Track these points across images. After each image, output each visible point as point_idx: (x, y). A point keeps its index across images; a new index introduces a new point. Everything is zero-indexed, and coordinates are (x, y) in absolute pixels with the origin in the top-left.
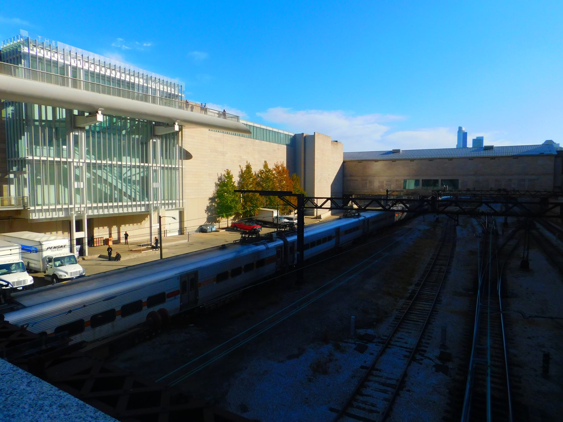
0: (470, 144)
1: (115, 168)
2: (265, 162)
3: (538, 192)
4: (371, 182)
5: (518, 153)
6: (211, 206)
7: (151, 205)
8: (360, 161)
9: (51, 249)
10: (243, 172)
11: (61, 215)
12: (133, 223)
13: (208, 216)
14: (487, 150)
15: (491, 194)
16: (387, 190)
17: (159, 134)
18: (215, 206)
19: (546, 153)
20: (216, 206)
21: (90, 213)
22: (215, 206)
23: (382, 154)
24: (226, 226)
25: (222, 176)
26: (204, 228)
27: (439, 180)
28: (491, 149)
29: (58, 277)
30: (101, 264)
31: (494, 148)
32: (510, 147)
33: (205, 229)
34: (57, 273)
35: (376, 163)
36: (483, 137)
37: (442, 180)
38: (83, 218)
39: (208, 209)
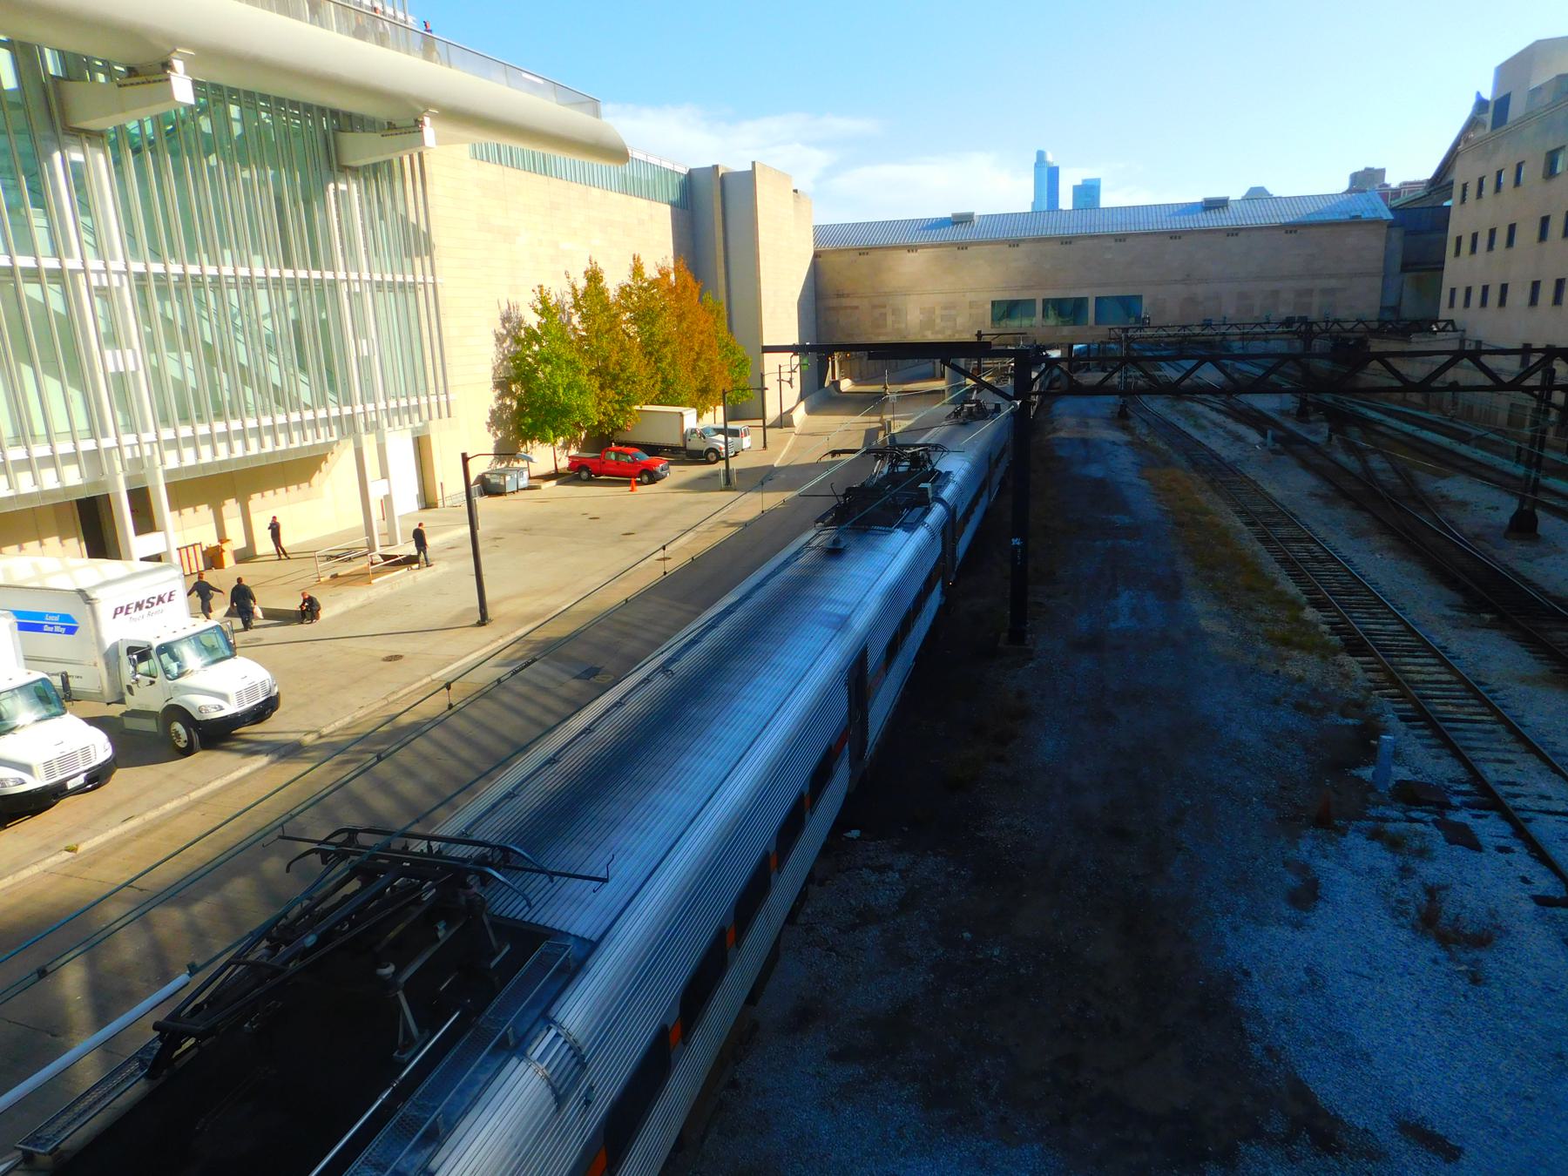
0: (1066, 202)
1: (233, 292)
2: (636, 259)
3: (1257, 324)
4: (896, 311)
5: (1296, 217)
6: (503, 407)
7: (370, 414)
8: (863, 251)
9: (127, 613)
10: (580, 293)
11: (73, 477)
12: (286, 483)
13: (496, 442)
14: (1212, 211)
15: (1267, 333)
16: (980, 332)
17: (361, 162)
18: (511, 406)
19: (1366, 215)
20: (515, 407)
21: (172, 461)
22: (511, 406)
23: (924, 229)
24: (550, 468)
25: (512, 310)
26: (493, 481)
27: (1090, 300)
28: (1222, 207)
29: (194, 716)
30: (260, 639)
31: (975, 218)
32: (1153, 207)
33: (498, 485)
34: (184, 701)
35: (912, 255)
36: (1099, 180)
37: (1098, 299)
38: (149, 484)
39: (496, 420)
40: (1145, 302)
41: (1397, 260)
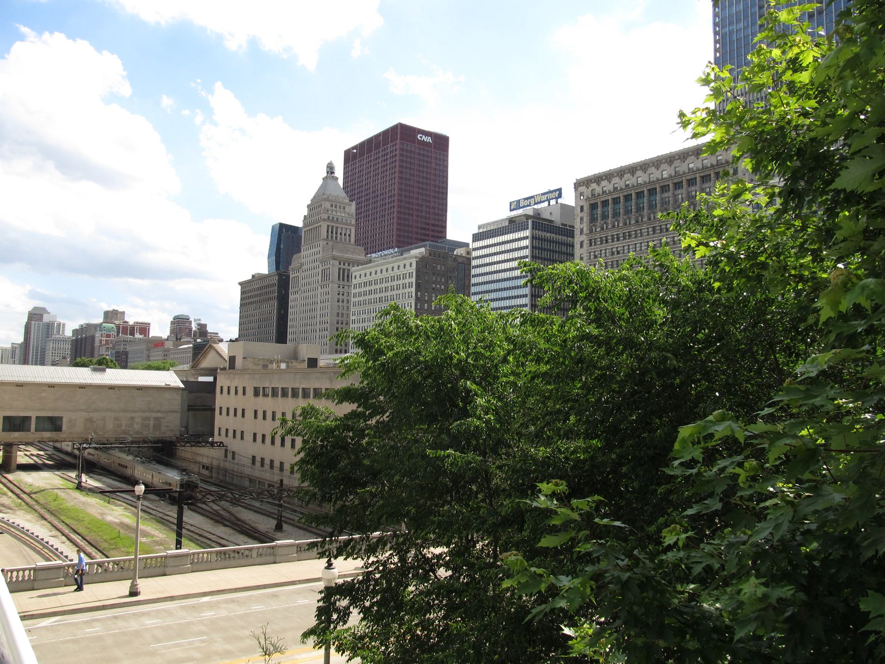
37: (37, 418)
40: (65, 420)
41: (186, 408)
